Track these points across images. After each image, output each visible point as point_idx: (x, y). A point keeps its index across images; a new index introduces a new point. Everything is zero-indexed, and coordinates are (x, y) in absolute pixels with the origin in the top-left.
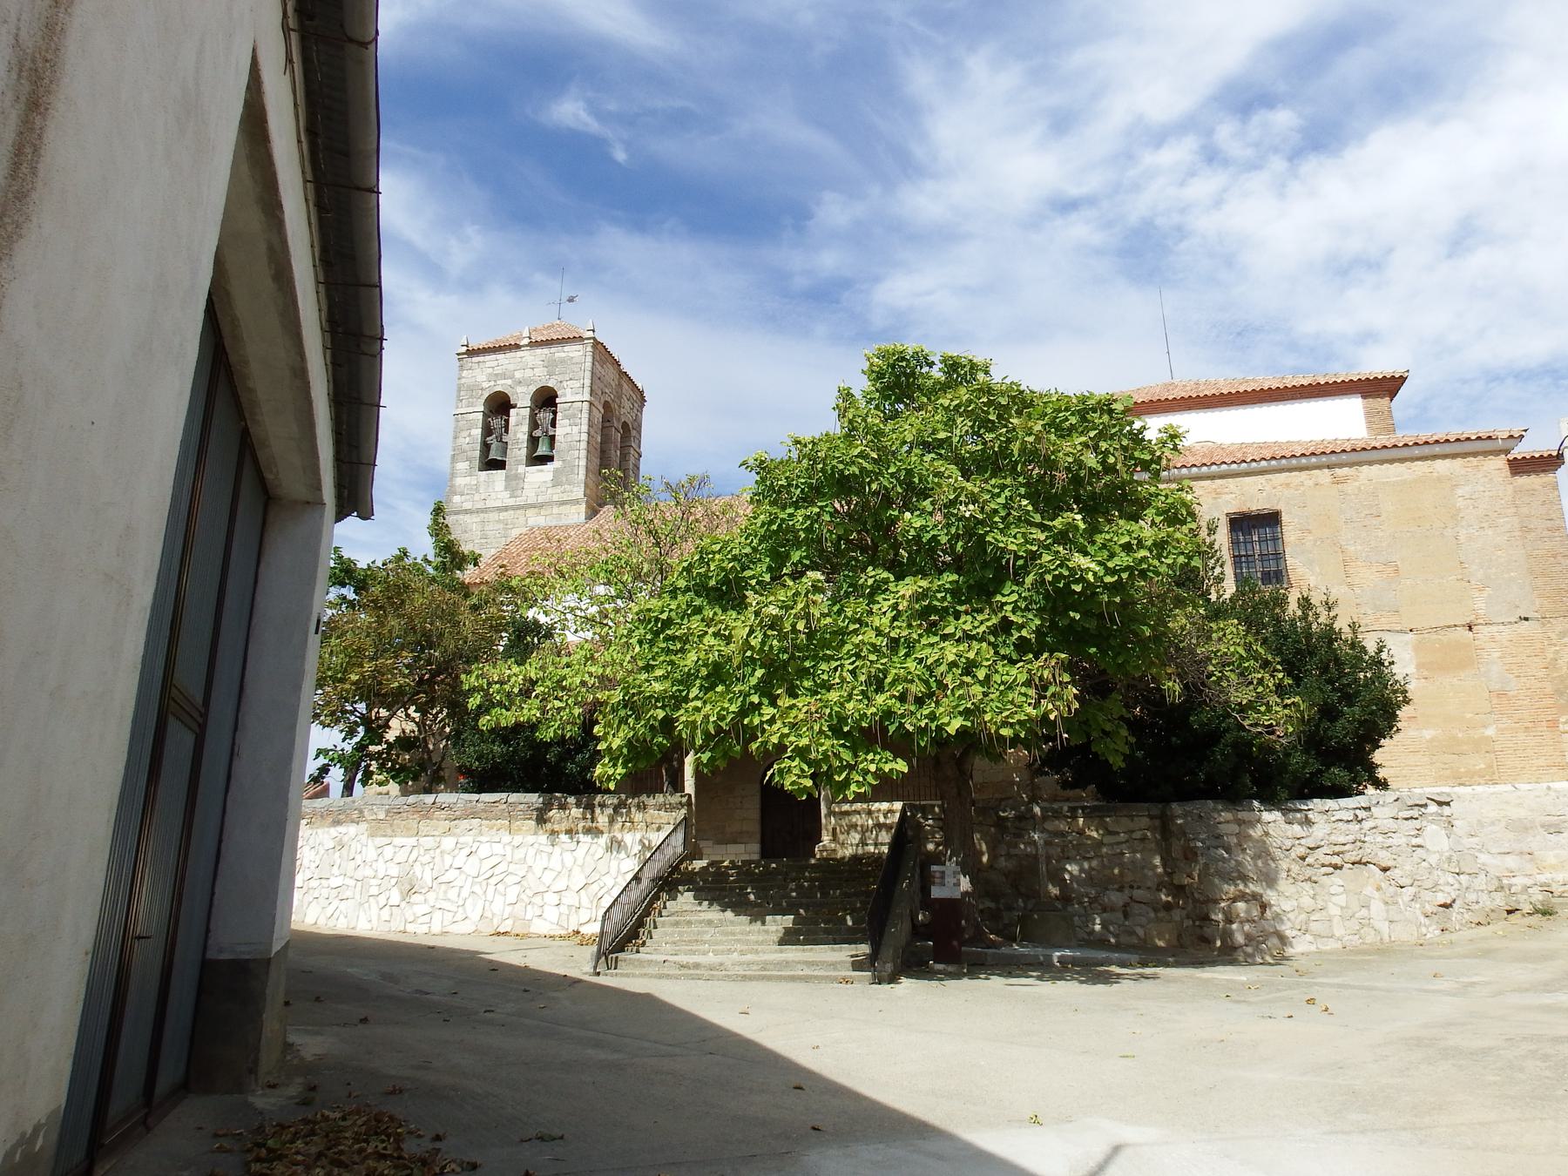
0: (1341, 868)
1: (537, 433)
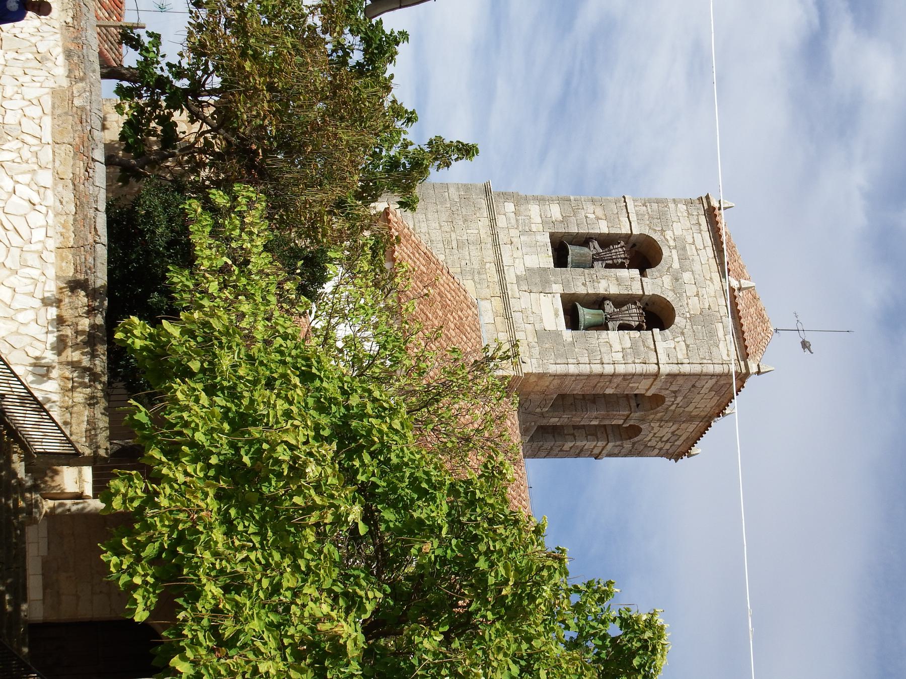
1: (609, 307)
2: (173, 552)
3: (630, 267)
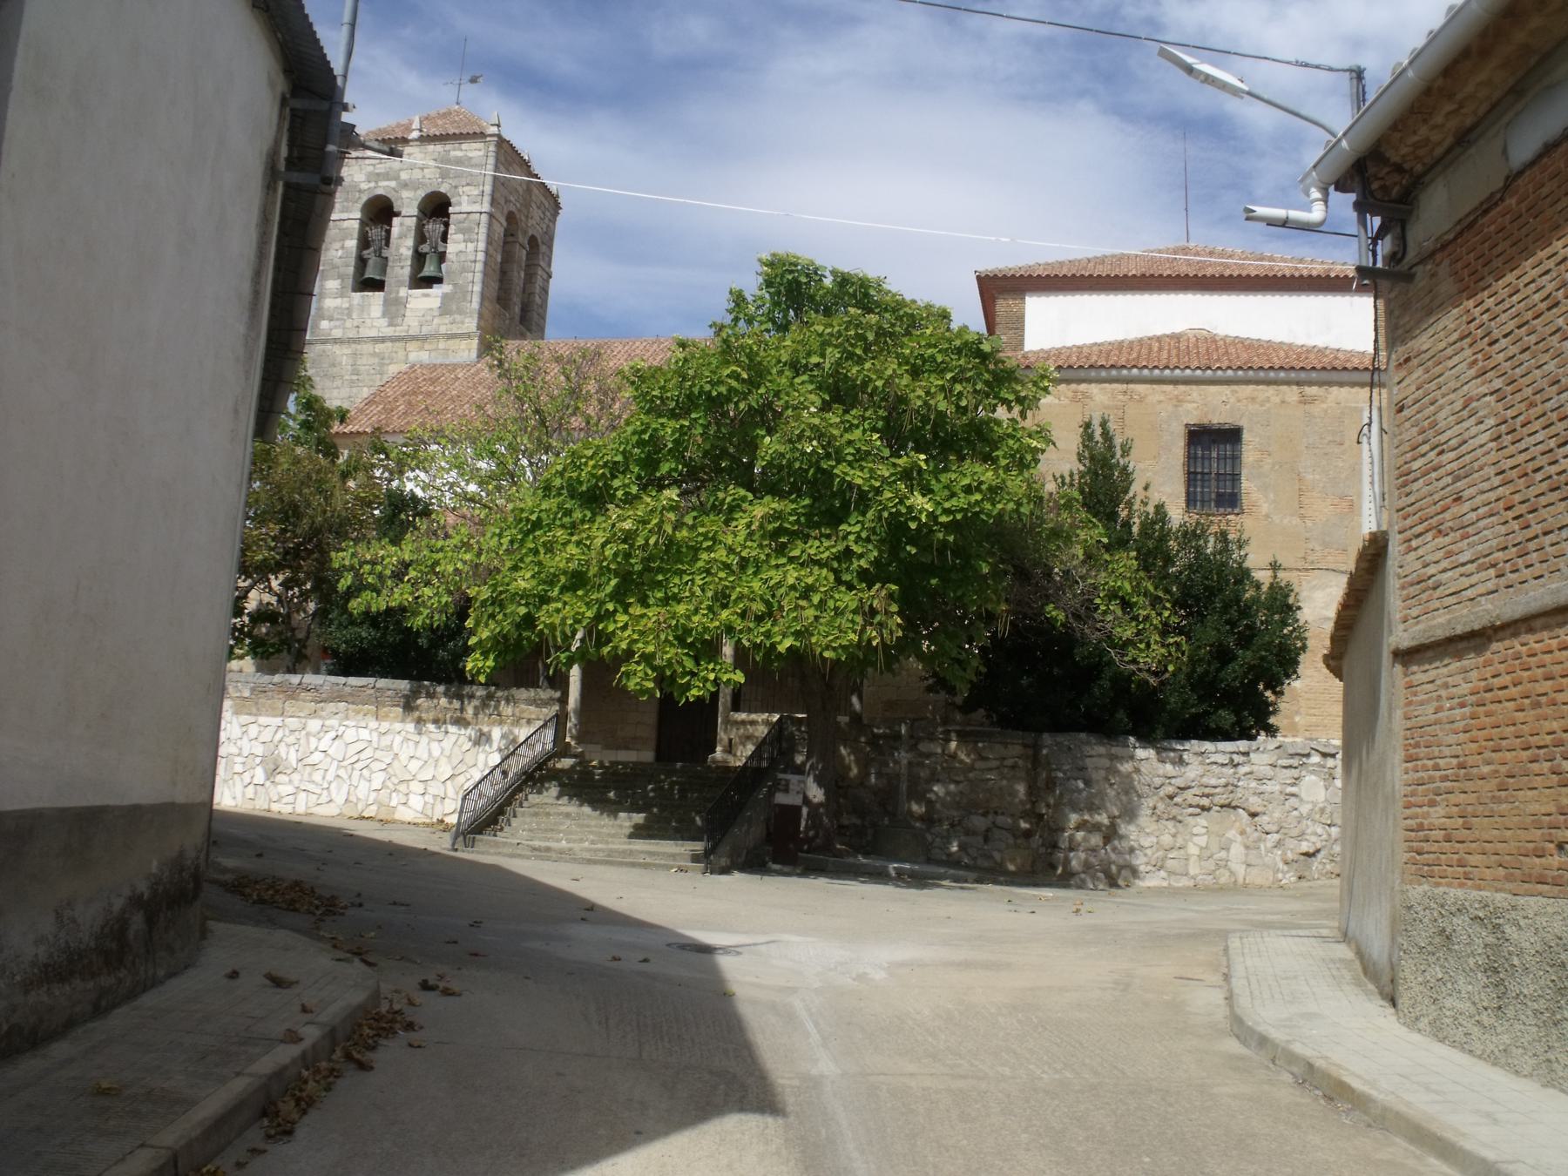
0: (1209, 809)
1: (425, 248)
2: (690, 646)
3: (390, 224)
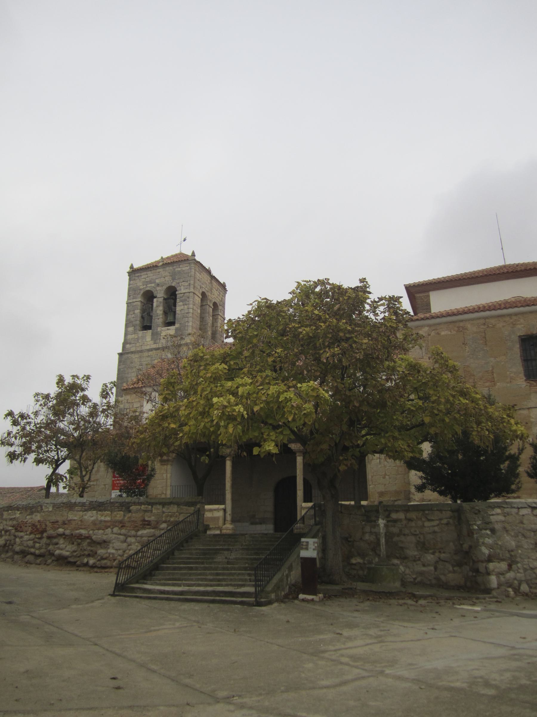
3: (153, 302)
